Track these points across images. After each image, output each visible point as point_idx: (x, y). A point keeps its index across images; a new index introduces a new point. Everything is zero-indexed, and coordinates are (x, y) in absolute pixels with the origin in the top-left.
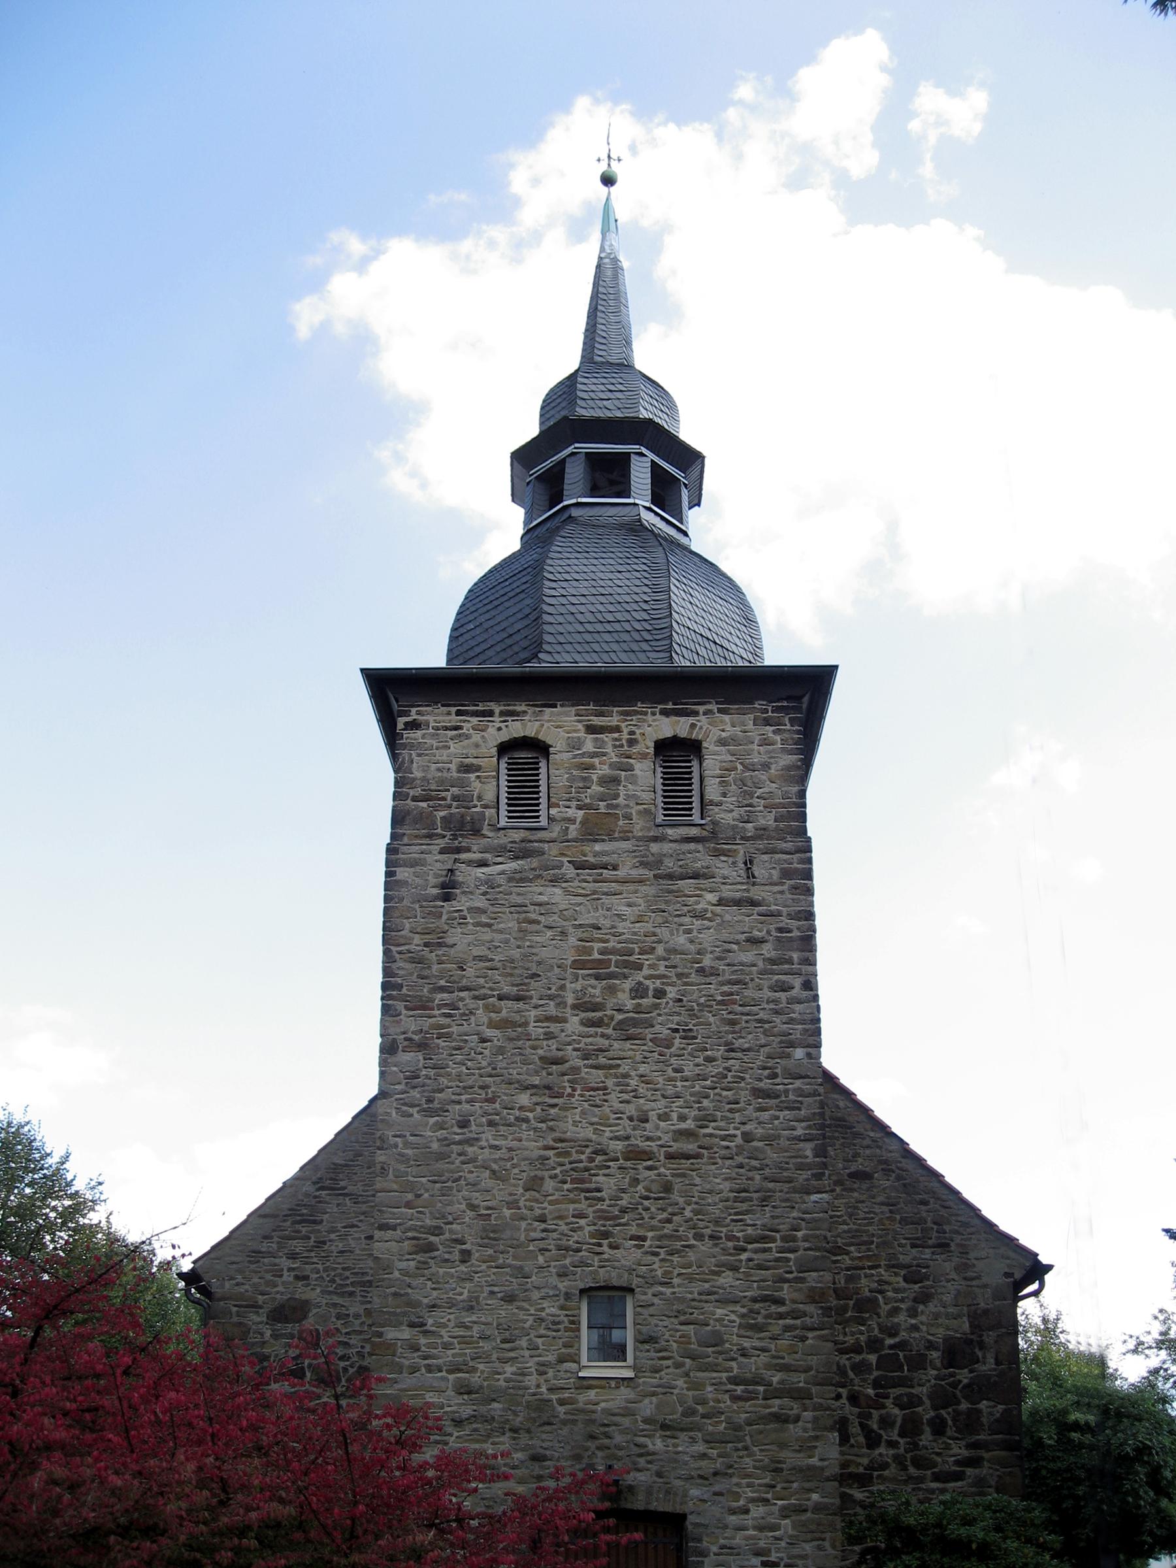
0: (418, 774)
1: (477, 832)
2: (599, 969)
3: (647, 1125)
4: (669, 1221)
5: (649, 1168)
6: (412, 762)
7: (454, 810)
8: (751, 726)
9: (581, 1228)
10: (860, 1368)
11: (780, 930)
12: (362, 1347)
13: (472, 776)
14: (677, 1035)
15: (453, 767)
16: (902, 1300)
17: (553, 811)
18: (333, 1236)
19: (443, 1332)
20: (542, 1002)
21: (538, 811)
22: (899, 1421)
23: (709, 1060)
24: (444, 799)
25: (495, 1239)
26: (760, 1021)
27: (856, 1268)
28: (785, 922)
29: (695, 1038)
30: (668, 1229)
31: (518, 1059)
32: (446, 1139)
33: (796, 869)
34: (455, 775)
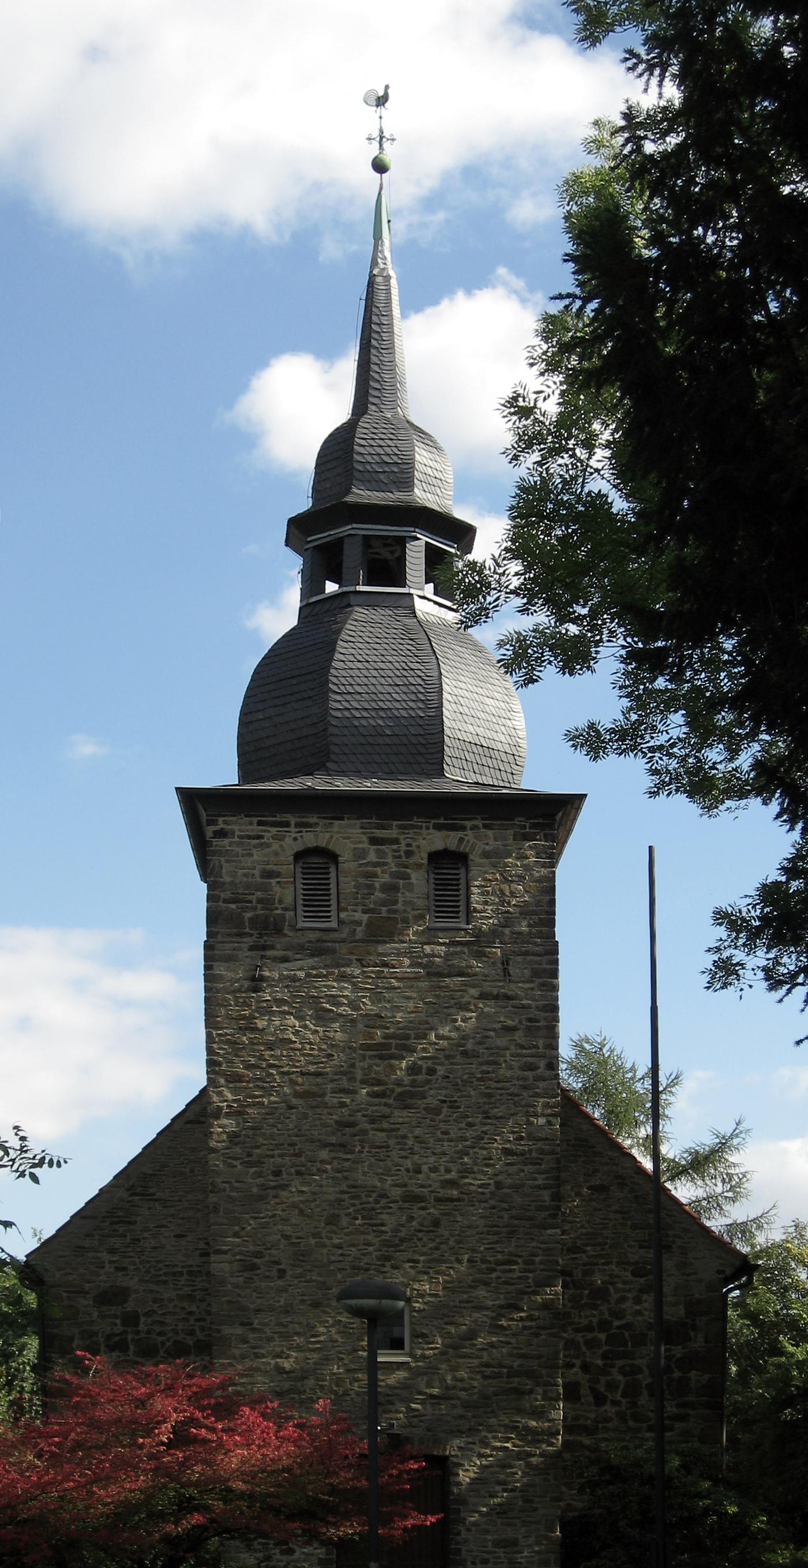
0: (227, 879)
1: (279, 931)
2: (384, 1052)
3: (420, 1176)
4: (437, 1249)
5: (423, 1208)
6: (221, 867)
7: (259, 912)
8: (511, 841)
9: (369, 1253)
10: (591, 1344)
11: (530, 1020)
12: (176, 1325)
13: (273, 881)
14: (445, 1105)
15: (257, 872)
16: (629, 1291)
17: (343, 915)
18: (146, 1235)
19: (267, 1329)
20: (336, 1077)
21: (329, 912)
22: (622, 1386)
23: (470, 1125)
24: (250, 902)
25: (303, 1261)
26: (511, 1095)
27: (591, 1264)
28: (534, 1013)
29: (459, 1107)
30: (436, 1254)
31: (318, 1123)
32: (263, 1185)
33: (545, 969)
34: (259, 879)
